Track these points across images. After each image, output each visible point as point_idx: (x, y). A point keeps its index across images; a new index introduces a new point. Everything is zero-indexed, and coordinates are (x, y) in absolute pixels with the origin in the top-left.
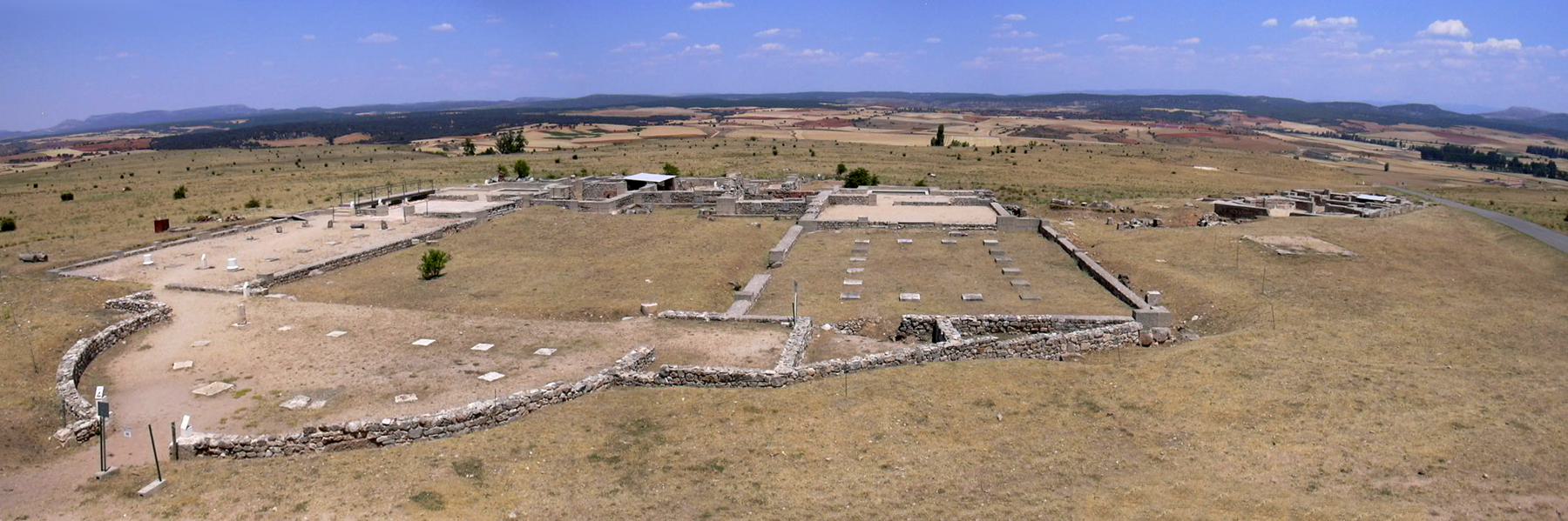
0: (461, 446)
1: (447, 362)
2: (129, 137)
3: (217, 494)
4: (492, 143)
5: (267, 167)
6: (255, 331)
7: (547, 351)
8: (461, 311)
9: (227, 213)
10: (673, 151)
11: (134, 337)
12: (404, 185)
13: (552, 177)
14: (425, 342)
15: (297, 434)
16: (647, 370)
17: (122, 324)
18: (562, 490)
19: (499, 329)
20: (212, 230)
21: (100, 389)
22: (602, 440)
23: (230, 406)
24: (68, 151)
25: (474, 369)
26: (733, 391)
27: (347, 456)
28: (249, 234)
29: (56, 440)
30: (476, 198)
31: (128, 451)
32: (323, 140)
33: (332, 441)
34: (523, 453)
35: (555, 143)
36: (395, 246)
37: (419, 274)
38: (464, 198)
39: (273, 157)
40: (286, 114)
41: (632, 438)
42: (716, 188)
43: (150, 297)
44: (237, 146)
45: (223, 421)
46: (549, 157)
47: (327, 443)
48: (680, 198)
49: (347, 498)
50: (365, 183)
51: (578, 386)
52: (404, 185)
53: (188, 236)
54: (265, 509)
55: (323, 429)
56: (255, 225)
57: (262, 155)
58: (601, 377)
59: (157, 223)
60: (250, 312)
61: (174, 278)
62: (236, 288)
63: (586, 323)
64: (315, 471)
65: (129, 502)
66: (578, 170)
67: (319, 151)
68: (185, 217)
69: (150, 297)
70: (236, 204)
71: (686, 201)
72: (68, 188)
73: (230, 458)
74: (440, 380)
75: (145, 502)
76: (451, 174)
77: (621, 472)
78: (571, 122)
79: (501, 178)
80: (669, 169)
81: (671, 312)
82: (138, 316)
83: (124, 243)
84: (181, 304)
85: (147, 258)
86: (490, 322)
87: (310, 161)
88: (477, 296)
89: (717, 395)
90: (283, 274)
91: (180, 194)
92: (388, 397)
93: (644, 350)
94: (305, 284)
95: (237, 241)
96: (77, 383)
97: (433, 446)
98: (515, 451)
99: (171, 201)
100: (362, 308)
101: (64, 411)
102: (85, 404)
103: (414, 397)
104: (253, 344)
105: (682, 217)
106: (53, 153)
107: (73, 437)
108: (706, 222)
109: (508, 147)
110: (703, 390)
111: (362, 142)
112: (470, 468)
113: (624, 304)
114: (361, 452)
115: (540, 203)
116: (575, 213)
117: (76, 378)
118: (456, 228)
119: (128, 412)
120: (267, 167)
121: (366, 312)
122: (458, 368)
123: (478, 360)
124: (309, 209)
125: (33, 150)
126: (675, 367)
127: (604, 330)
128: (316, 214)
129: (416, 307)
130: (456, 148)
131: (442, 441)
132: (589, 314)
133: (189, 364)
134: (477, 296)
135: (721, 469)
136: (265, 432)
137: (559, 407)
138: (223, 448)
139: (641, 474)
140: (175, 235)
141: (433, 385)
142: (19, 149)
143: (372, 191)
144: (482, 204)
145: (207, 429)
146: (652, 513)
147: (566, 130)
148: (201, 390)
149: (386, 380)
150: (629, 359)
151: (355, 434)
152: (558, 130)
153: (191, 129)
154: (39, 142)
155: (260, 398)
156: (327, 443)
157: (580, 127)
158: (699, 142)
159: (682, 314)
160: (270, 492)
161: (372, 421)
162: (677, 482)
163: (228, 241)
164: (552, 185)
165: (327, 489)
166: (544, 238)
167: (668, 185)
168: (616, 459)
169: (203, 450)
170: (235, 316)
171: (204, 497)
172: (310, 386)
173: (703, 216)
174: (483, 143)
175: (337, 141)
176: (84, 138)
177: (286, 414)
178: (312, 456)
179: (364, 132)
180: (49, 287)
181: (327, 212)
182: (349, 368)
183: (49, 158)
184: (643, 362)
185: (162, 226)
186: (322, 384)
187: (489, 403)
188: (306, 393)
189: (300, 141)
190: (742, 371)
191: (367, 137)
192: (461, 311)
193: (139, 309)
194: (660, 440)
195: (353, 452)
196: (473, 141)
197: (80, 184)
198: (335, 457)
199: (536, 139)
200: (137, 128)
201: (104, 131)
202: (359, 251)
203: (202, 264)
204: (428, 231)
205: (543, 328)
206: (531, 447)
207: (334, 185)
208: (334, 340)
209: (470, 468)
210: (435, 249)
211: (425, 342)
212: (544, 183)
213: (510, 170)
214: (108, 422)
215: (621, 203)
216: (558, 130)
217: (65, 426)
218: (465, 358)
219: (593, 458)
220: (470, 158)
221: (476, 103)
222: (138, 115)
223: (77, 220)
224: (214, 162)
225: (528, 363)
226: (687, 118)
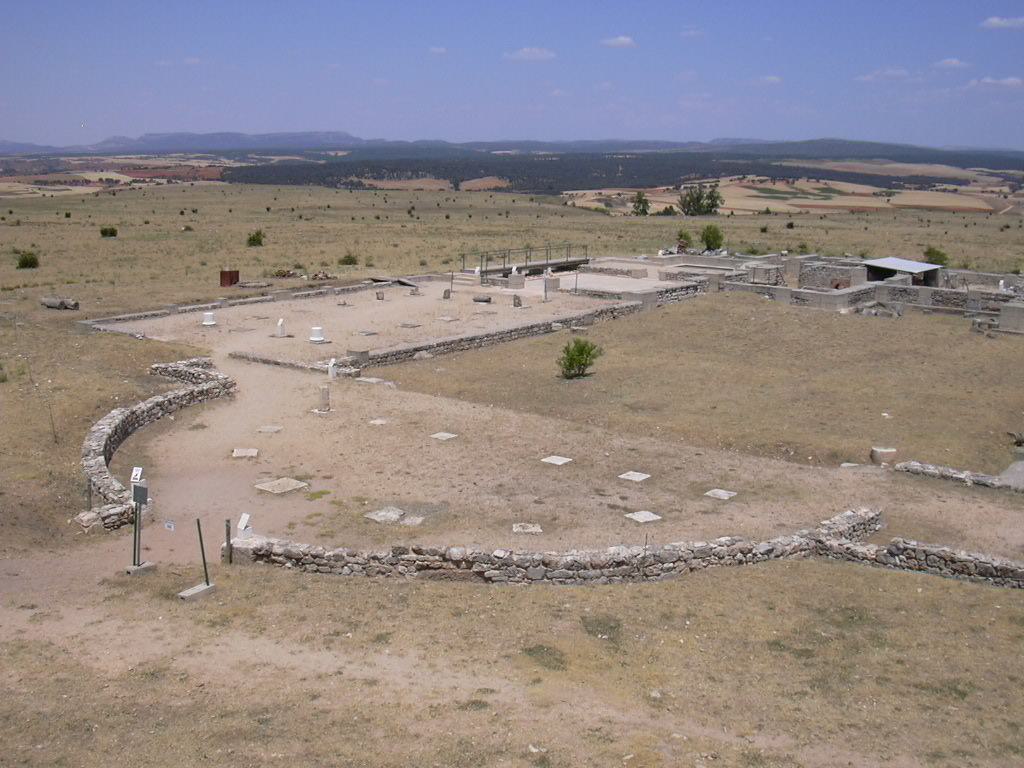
0: (594, 598)
1: (585, 489)
2: (194, 163)
3: (278, 609)
4: (673, 200)
5: (370, 215)
6: (340, 422)
7: (723, 494)
8: (609, 426)
9: (316, 268)
10: (940, 230)
11: (185, 412)
12: (548, 249)
13: (754, 252)
14: (559, 461)
15: (384, 553)
16: (866, 541)
17: (171, 395)
18: (727, 677)
19: (659, 455)
20: (294, 289)
21: (137, 472)
22: (790, 624)
23: (301, 509)
24: (114, 176)
25: (620, 503)
26: (996, 590)
27: (445, 588)
28: (342, 298)
29: (79, 525)
30: (644, 274)
31: (168, 545)
32: (445, 184)
33: (428, 567)
34: (677, 622)
35: (762, 204)
36: (529, 331)
37: (558, 370)
38: (628, 273)
39: (379, 201)
40: (400, 147)
41: (834, 630)
42: (1002, 289)
43: (209, 365)
44: (333, 185)
45: (291, 525)
46: (752, 223)
47: (420, 568)
48: (942, 299)
49: (441, 637)
50: (497, 244)
51: (763, 547)
52: (548, 249)
53: (263, 293)
54: (337, 634)
55: (418, 552)
56: (350, 287)
57: (366, 197)
58: (797, 540)
59: (223, 274)
60: (336, 397)
61: (241, 345)
62: (319, 365)
63: (783, 463)
64: (404, 599)
65: (166, 604)
66: (795, 245)
67: (440, 198)
68: (261, 270)
69: (209, 365)
70: (326, 259)
71: (955, 305)
72: (111, 221)
73: (297, 570)
74: (574, 511)
75: (186, 606)
76: (613, 239)
77: (814, 672)
78: (789, 175)
79: (682, 248)
80: (932, 256)
81: (915, 465)
82: (191, 387)
83: (180, 296)
84: (246, 377)
85: (208, 317)
86: (648, 444)
87: (428, 209)
88: (634, 408)
89: (972, 593)
90: (380, 352)
91: (255, 240)
92: (505, 523)
93: (865, 512)
94: (406, 370)
95: (325, 306)
96: (108, 460)
97: (557, 592)
98: (667, 617)
99: (243, 248)
100: (480, 407)
101: (89, 492)
102: (117, 486)
103: (537, 529)
104: (336, 437)
105: (945, 328)
106: (93, 176)
107: (99, 523)
108: (982, 338)
109: (698, 206)
110: (951, 582)
111: (497, 189)
112: (605, 628)
113: (845, 444)
114: (463, 586)
115: (734, 288)
116: (785, 306)
117: (108, 453)
118: (612, 313)
119: (169, 501)
120: (370, 215)
121: (484, 413)
122: (599, 499)
123: (627, 493)
124: (421, 272)
125: (67, 171)
126: (913, 544)
127: (811, 477)
128: (430, 279)
129: (550, 413)
130: (623, 204)
131: (570, 588)
132: (793, 453)
133: (254, 452)
134: (634, 408)
135: (963, 695)
136: (343, 545)
137: (734, 570)
138: (289, 557)
139: (843, 680)
140: (246, 292)
141: (564, 516)
142: (48, 167)
143: (504, 255)
144: (652, 283)
145: (271, 533)
146: (854, 733)
147: (780, 186)
148: (267, 485)
149: (503, 503)
150: (841, 520)
151: (457, 563)
152: (769, 185)
153: (276, 159)
154: (74, 161)
155: (340, 504)
156: (420, 568)
157: (802, 184)
158: (980, 219)
159: (931, 469)
160: (344, 615)
161: (481, 550)
162: (897, 701)
163: (313, 305)
164: (752, 264)
165: (417, 623)
166: (734, 337)
167: (928, 278)
168: (807, 653)
169: (263, 555)
170: (316, 399)
171: (262, 610)
172: (404, 497)
173: (978, 329)
174: (661, 200)
175: (464, 185)
176: (135, 160)
177: (372, 526)
178: (401, 581)
179: (501, 175)
180: (79, 342)
181: (443, 278)
182: (456, 480)
183: (87, 182)
184: (862, 529)
185: (230, 278)
186: (420, 496)
187: (636, 550)
188: (399, 505)
189: (417, 183)
190: (1013, 565)
191: (504, 184)
192: (609, 426)
193: (194, 379)
194: (878, 641)
195: (454, 584)
196: (647, 196)
197: (127, 218)
198: (430, 587)
199: (734, 197)
200: (205, 153)
201: (161, 153)
202: (481, 333)
203: (278, 332)
204: (575, 313)
205: (723, 461)
206: (689, 615)
207: (456, 243)
208: (440, 443)
209: (605, 628)
210: (582, 338)
211: (559, 461)
212: (742, 259)
213: (695, 238)
214: (145, 510)
215: (856, 299)
216: (769, 185)
217: (89, 508)
218: (610, 489)
219: (775, 645)
220: (641, 219)
221: (656, 144)
222: (212, 137)
223: (119, 262)
224: (302, 203)
225: (693, 506)
226: (965, 182)
